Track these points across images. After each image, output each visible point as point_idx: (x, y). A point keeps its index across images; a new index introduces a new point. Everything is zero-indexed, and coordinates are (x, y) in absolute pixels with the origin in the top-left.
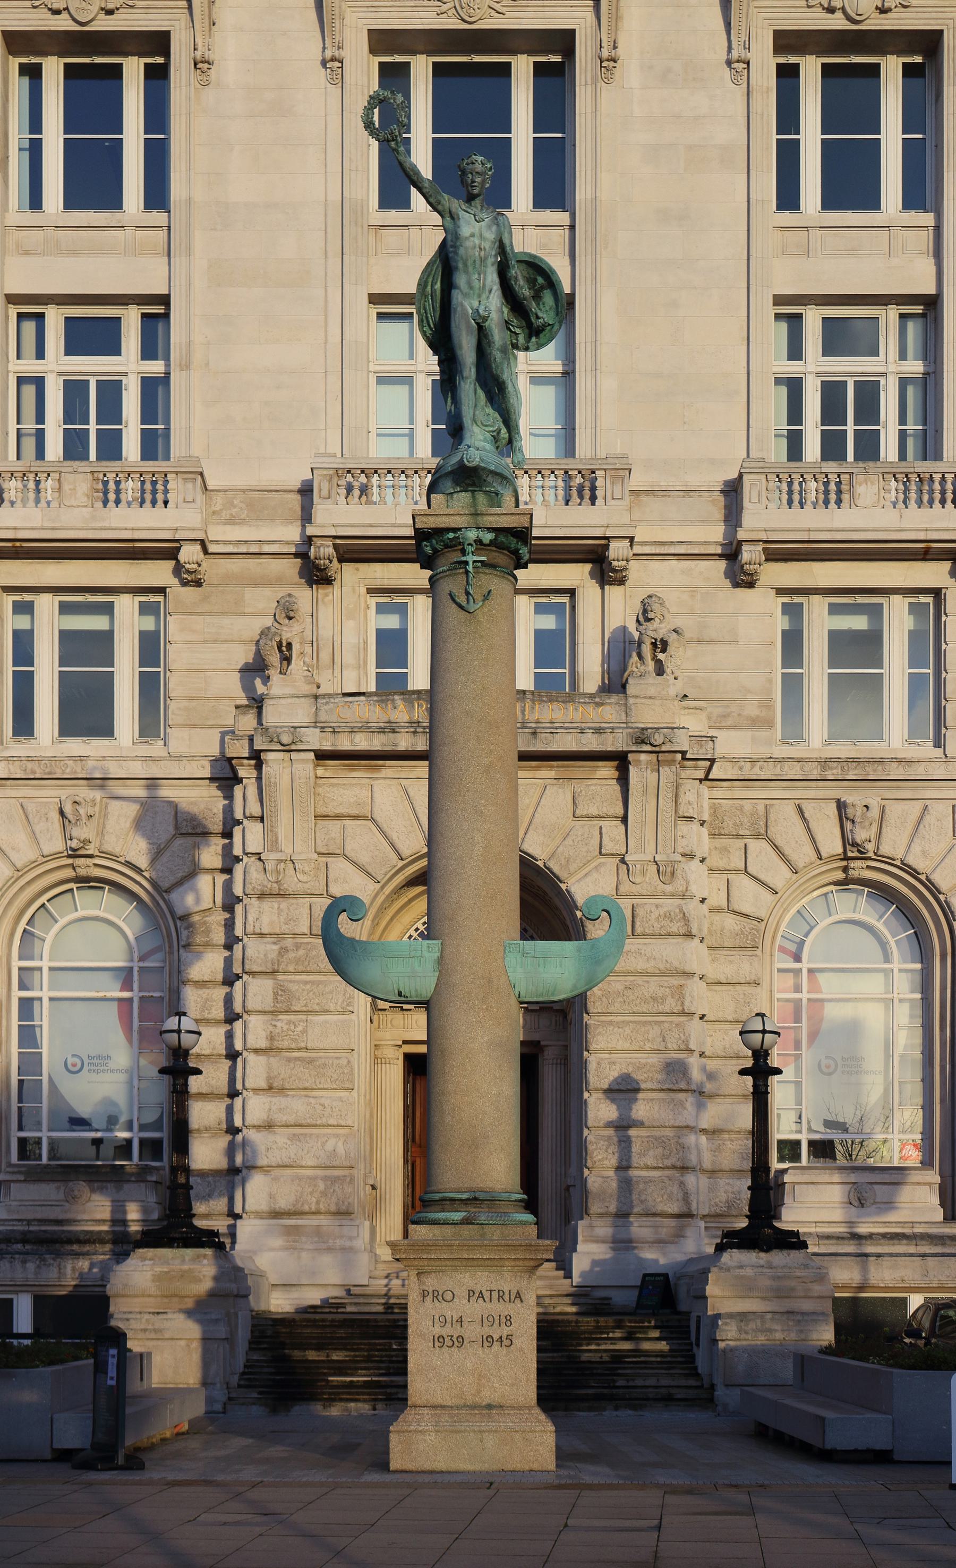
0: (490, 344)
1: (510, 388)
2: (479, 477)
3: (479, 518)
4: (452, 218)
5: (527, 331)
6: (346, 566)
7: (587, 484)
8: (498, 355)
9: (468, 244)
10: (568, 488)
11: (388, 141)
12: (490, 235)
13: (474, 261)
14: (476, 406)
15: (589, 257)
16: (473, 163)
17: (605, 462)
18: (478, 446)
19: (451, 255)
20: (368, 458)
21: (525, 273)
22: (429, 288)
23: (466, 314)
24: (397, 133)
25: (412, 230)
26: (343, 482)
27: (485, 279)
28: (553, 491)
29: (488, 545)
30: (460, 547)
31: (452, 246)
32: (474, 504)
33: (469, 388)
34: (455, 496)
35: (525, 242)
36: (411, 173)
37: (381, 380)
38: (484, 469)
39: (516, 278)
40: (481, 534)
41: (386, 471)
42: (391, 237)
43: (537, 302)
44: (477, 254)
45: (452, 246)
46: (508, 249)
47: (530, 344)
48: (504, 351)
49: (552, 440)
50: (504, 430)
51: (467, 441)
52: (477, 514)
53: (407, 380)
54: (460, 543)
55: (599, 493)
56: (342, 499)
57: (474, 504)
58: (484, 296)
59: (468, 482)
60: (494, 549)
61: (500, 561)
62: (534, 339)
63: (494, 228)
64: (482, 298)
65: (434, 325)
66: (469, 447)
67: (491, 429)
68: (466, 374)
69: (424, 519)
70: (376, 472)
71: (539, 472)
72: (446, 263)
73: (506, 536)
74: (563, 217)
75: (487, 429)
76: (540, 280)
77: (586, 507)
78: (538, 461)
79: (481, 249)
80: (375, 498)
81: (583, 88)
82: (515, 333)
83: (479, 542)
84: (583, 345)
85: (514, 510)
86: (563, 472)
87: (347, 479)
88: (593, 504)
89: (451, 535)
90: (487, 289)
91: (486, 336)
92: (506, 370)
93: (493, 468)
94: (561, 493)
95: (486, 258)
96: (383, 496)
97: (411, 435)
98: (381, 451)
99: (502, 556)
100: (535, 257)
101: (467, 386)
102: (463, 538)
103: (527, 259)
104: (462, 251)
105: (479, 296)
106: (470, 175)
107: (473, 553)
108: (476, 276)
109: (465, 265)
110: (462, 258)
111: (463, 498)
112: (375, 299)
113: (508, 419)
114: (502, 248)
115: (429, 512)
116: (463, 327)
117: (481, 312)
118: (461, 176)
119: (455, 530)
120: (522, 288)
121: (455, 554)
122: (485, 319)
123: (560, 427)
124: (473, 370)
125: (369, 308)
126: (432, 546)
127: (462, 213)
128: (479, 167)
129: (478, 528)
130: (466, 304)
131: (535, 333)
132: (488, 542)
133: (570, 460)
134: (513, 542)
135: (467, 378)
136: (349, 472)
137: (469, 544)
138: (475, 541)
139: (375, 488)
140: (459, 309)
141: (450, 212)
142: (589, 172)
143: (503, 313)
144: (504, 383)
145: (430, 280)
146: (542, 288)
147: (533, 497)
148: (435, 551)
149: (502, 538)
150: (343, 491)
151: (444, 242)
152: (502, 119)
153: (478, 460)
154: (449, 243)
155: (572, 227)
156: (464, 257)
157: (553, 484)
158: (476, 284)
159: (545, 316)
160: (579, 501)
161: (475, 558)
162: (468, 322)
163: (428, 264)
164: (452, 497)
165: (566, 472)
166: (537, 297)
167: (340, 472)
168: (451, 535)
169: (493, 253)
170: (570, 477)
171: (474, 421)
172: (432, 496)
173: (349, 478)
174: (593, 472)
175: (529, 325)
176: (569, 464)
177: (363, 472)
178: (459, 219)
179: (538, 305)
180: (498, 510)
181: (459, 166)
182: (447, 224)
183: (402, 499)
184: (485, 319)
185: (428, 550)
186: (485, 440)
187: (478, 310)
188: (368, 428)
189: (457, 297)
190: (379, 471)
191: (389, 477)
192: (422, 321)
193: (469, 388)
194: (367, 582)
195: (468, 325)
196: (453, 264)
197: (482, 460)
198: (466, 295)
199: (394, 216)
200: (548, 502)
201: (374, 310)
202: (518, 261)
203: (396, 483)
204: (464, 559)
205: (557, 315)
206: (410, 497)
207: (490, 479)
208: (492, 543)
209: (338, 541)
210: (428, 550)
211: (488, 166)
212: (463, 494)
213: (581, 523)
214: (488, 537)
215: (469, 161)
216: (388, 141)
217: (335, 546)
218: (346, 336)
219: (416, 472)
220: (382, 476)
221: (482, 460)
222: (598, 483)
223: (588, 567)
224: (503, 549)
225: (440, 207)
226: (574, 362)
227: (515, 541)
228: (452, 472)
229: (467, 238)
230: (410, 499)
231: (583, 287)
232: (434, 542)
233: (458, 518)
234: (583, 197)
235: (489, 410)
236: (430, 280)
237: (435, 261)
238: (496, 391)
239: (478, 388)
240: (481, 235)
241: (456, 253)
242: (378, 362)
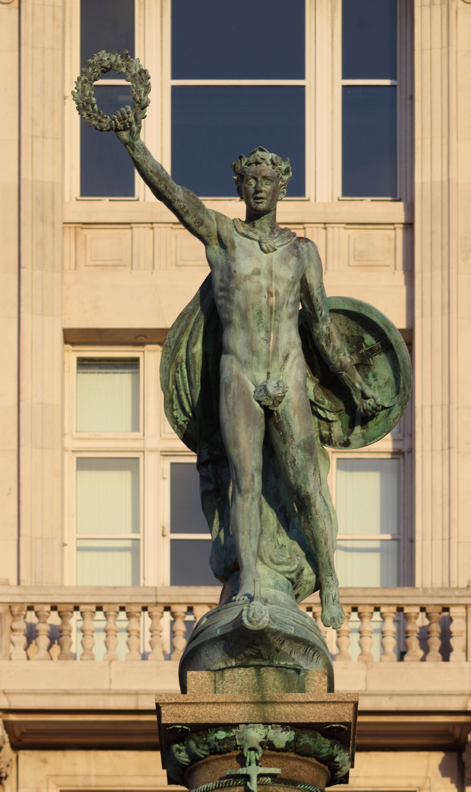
0: (284, 438)
1: (318, 505)
2: (269, 646)
3: (269, 709)
4: (223, 245)
5: (346, 417)
6: (28, 759)
7: (436, 629)
8: (299, 456)
9: (250, 286)
10: (403, 635)
11: (117, 130)
12: (287, 272)
13: (260, 312)
14: (261, 533)
15: (438, 274)
16: (257, 163)
17: (465, 593)
18: (267, 594)
19: (220, 302)
20: (62, 586)
21: (344, 329)
22: (183, 352)
23: (245, 393)
24: (132, 119)
25: (137, 230)
26: (21, 625)
27: (277, 339)
28: (377, 638)
29: (284, 750)
30: (237, 753)
31: (222, 289)
32: (260, 686)
33: (252, 511)
34: (228, 673)
35: (340, 283)
36: (156, 179)
37: (84, 464)
38: (276, 633)
39: (329, 337)
40: (272, 733)
41: (93, 608)
42: (103, 241)
43: (360, 368)
44: (264, 301)
45: (222, 289)
46: (316, 293)
47: (351, 438)
48: (309, 448)
49: (375, 558)
50: (308, 570)
51: (247, 588)
52: (266, 703)
53: (129, 464)
54: (236, 747)
55: (456, 643)
56: (18, 651)
57: (260, 686)
58: (276, 365)
59: (249, 652)
60: (293, 755)
61: (302, 774)
62: (358, 430)
63: (293, 261)
64: (270, 368)
65: (192, 408)
66: (251, 599)
67: (286, 568)
68: (245, 484)
69: (177, 710)
70: (76, 608)
71: (355, 609)
72: (212, 310)
73: (314, 736)
74: (395, 211)
75: (280, 568)
76: (369, 340)
77: (434, 663)
78: (351, 592)
79: (270, 294)
80: (76, 647)
81: (426, 11)
82: (327, 420)
83: (268, 745)
84: (427, 411)
85: (326, 697)
86: (394, 609)
87: (29, 620)
88: (446, 658)
89: (221, 735)
90: (281, 353)
91: (279, 426)
92: (311, 479)
93: (291, 631)
94: (391, 642)
95: (279, 308)
96: (88, 646)
97: (135, 549)
98: (82, 575)
99: (306, 767)
100: (361, 304)
101: (247, 504)
102: (242, 739)
103: (347, 307)
104: (238, 297)
105: (268, 365)
106: (253, 182)
107: (257, 762)
108: (263, 335)
109: (245, 318)
110: (239, 307)
111: (242, 677)
112: (72, 337)
113: (314, 553)
114: (305, 291)
115: (183, 698)
116: (241, 411)
117: (271, 389)
118: (237, 182)
119: (227, 727)
120: (338, 352)
121: (227, 764)
122: (278, 400)
123: (388, 537)
124: (258, 479)
125: (63, 350)
126: (188, 751)
127: (238, 239)
128: (267, 169)
129: (266, 724)
130: (246, 377)
131: (359, 418)
132: (283, 745)
133: (407, 591)
134: (325, 745)
135: (247, 491)
136: (30, 608)
137: (251, 749)
138: (261, 744)
139: (74, 634)
140: (234, 385)
141: (219, 237)
142: (437, 141)
143: (306, 389)
144: (308, 497)
145: (185, 339)
146: (372, 351)
147: (344, 648)
148: (194, 758)
149: (306, 739)
150: (21, 639)
151: (207, 286)
152: (293, 62)
153: (266, 619)
154: (217, 284)
155: (409, 226)
156: (243, 305)
157: (377, 626)
158: (262, 347)
159: (377, 394)
160: (421, 653)
161: (262, 770)
162: (249, 406)
163: (182, 315)
164: (222, 677)
165: (400, 609)
166: (364, 365)
167: (16, 609)
168: (221, 735)
169: (292, 299)
170: (406, 617)
171: (259, 556)
172: (190, 674)
173: (31, 617)
174: (446, 609)
175: (351, 408)
176: (404, 596)
177: (54, 608)
178: (234, 247)
179: (365, 377)
180: (300, 697)
181: (234, 168)
182: (213, 255)
183: (121, 649)
184: (278, 400)
185: (183, 757)
186: (277, 586)
187: (265, 388)
188: (62, 538)
189: (230, 366)
190: (82, 608)
191: (100, 615)
192: (172, 402)
193: (252, 511)
194: (61, 781)
195: (249, 411)
196: (224, 316)
197: (273, 619)
198: (245, 364)
199: (106, 208)
200: (370, 656)
201: (73, 354)
202: (332, 311)
203: (111, 626)
204: (242, 771)
205: (397, 393)
206: (134, 647)
207: (286, 648)
208: (289, 747)
209: (13, 718)
210: (183, 757)
211: (284, 167)
212: (241, 670)
213: (425, 689)
214: (282, 738)
215: (252, 159)
216: (117, 130)
217: (8, 726)
218: (25, 396)
219: (145, 609)
220: (87, 615)
221: (273, 619)
222: (454, 627)
223: (437, 758)
224: (308, 755)
225: (202, 230)
226: (412, 435)
227: (328, 743)
228: (223, 637)
229: (247, 277)
230: (134, 652)
231: (427, 319)
232: (192, 744)
233: (232, 708)
234: (427, 180)
235: (284, 539)
236: (185, 339)
237: (194, 311)
238: (294, 509)
239: (265, 505)
240: (271, 272)
241: (229, 299)
242: (80, 435)
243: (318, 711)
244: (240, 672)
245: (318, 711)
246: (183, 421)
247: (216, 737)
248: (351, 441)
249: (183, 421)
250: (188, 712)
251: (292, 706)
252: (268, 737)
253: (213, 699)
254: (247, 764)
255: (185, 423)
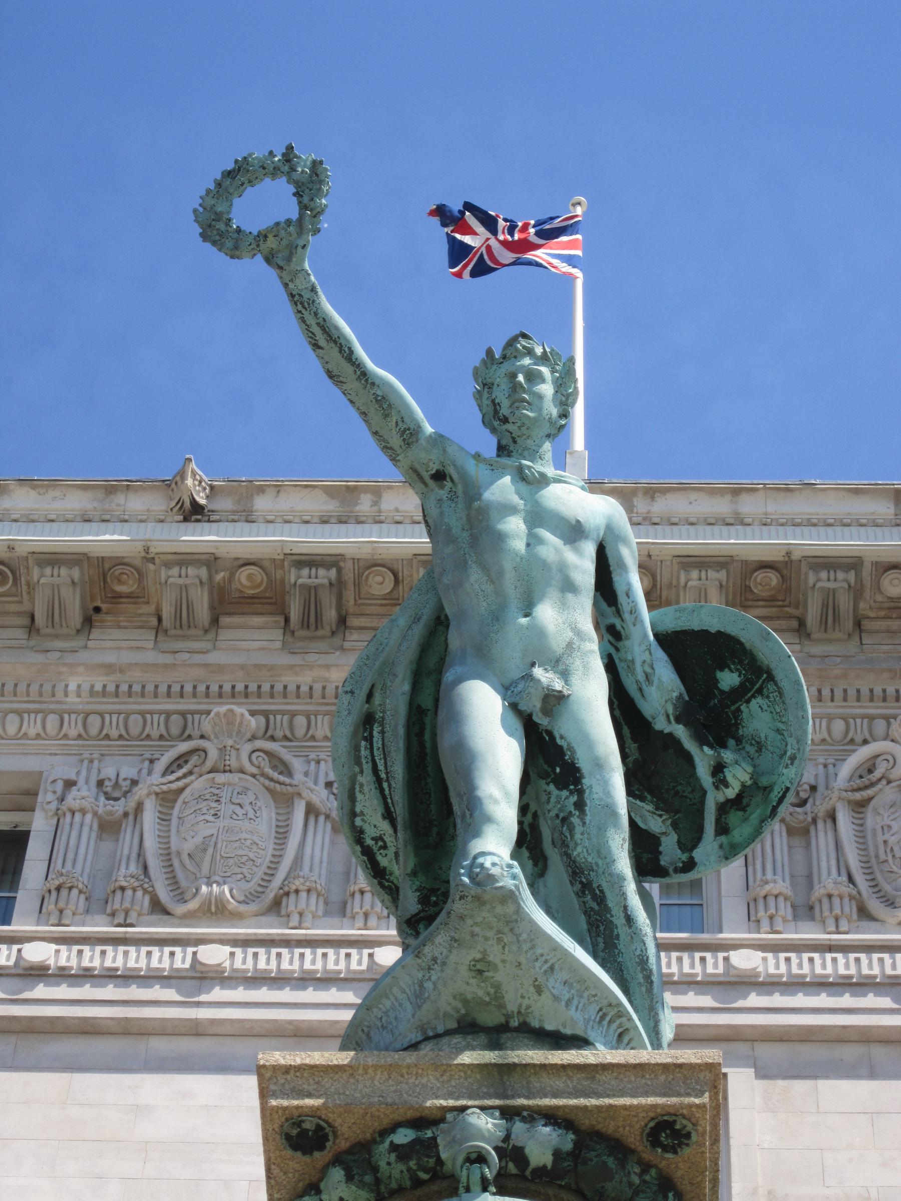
168: (404, 1136)
214: (542, 1144)
243: (630, 1086)
244: (455, 1041)
245: (630, 1086)
246: (373, 839)
247: (392, 1142)
248: (696, 860)
249: (373, 839)
250: (330, 1088)
251: (570, 1078)
252: (513, 1136)
253: (389, 1060)
254: (462, 1190)
255: (376, 843)
